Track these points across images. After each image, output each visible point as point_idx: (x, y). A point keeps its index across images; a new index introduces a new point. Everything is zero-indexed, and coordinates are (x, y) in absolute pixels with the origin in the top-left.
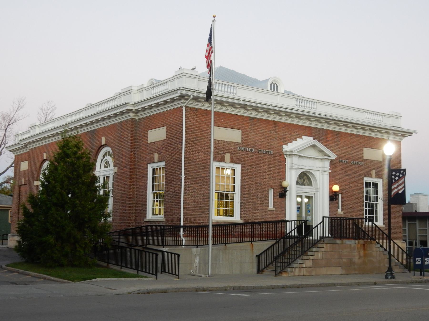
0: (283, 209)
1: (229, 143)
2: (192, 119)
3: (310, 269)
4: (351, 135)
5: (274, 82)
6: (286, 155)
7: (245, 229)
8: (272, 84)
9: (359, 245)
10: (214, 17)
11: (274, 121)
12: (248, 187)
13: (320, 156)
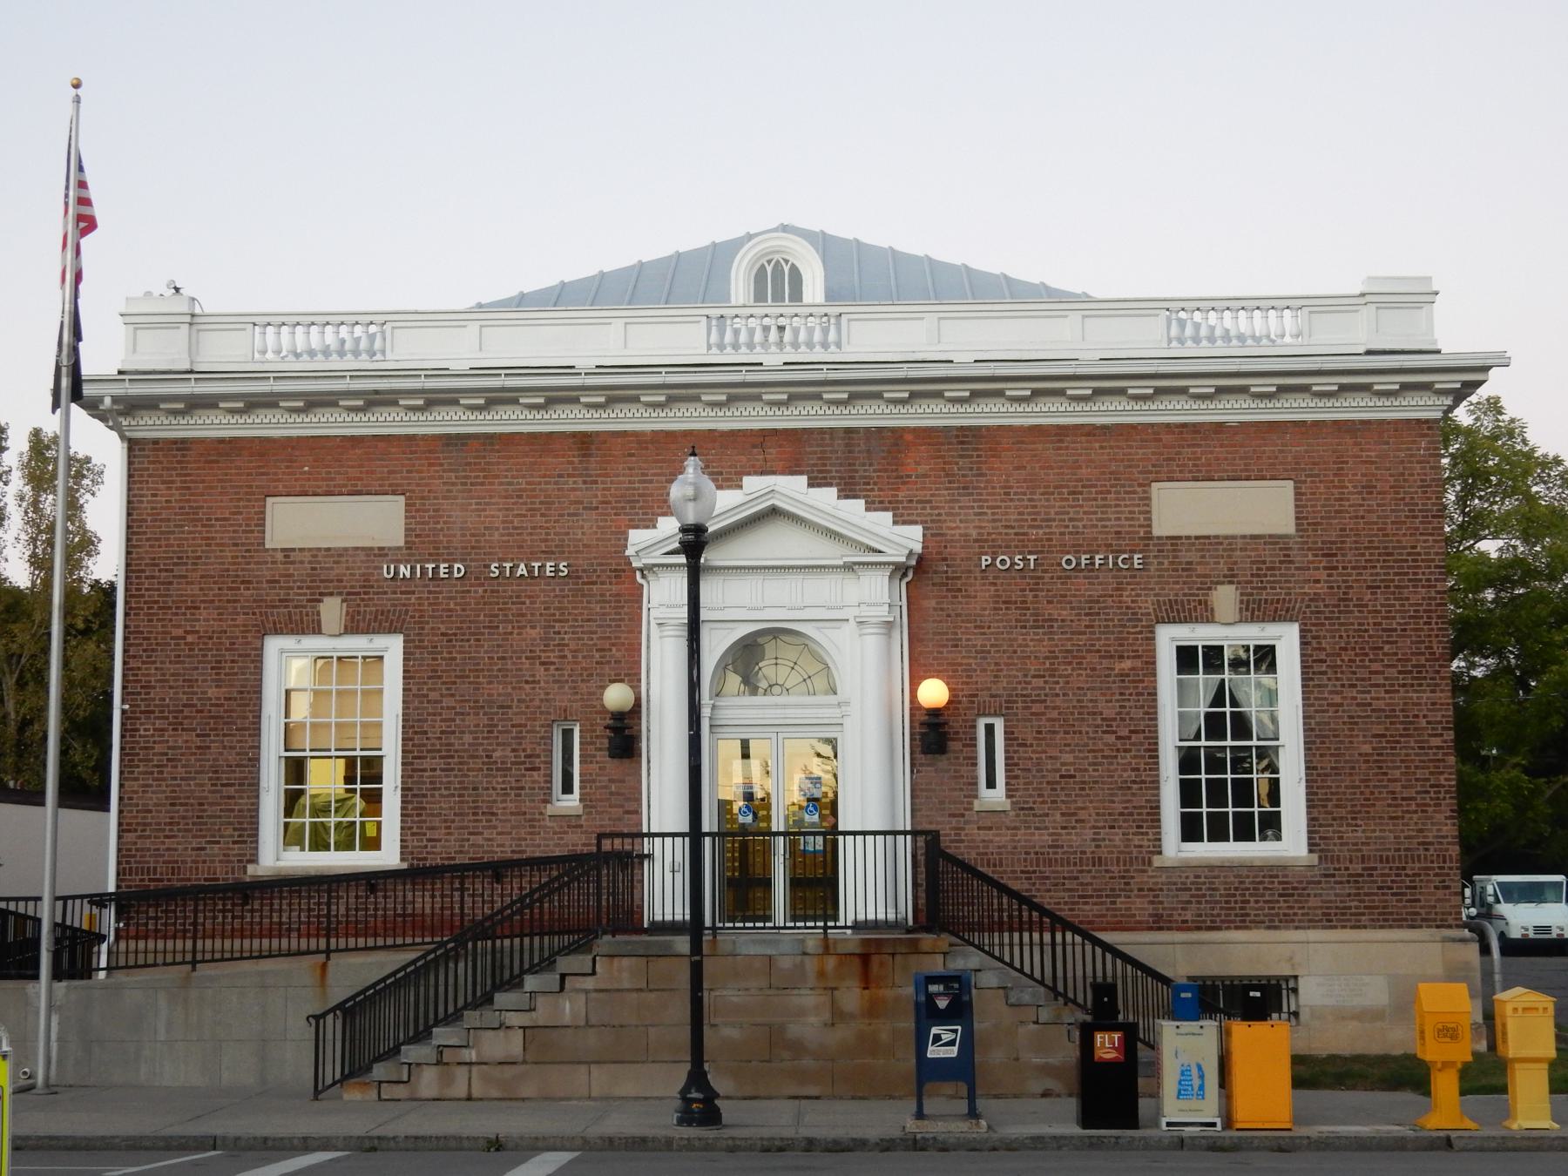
0: (631, 806)
1: (338, 554)
2: (164, 482)
3: (509, 1072)
5: (777, 257)
6: (641, 570)
7: (423, 901)
8: (769, 269)
10: (77, 86)
11: (574, 435)
12: (440, 726)
13: (833, 554)
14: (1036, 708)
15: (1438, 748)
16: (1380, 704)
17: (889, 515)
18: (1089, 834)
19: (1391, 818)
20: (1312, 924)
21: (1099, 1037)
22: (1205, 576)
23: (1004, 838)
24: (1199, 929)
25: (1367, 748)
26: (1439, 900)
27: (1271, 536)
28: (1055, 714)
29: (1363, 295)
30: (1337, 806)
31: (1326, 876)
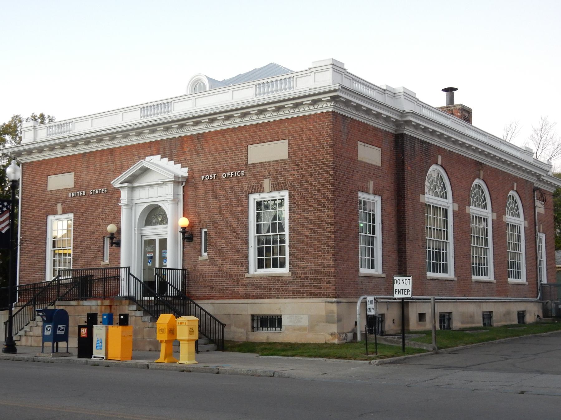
4: (224, 132)
9: (103, 308)
14: (216, 225)
15: (329, 232)
16: (311, 217)
17: (180, 165)
18: (228, 266)
19: (314, 258)
20: (289, 297)
21: (82, 329)
22: (262, 176)
23: (206, 269)
24: (257, 298)
25: (307, 234)
26: (327, 288)
27: (281, 160)
28: (220, 227)
29: (310, 69)
30: (298, 255)
31: (294, 279)
